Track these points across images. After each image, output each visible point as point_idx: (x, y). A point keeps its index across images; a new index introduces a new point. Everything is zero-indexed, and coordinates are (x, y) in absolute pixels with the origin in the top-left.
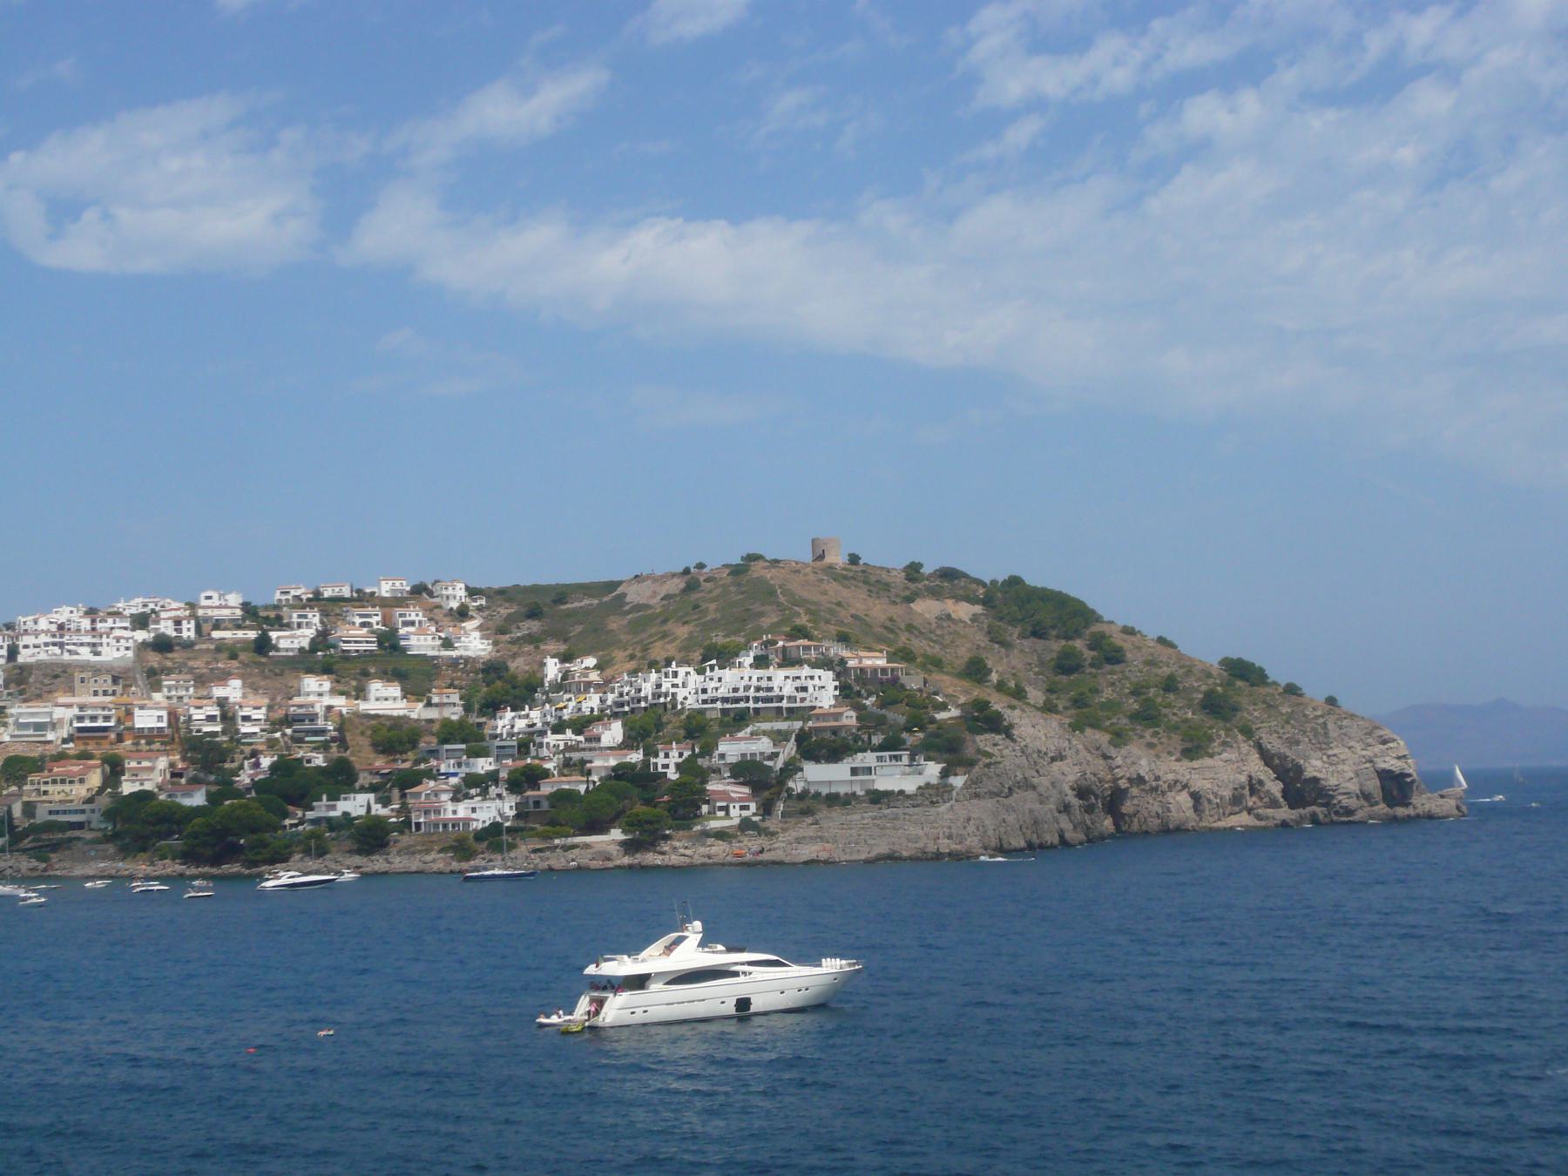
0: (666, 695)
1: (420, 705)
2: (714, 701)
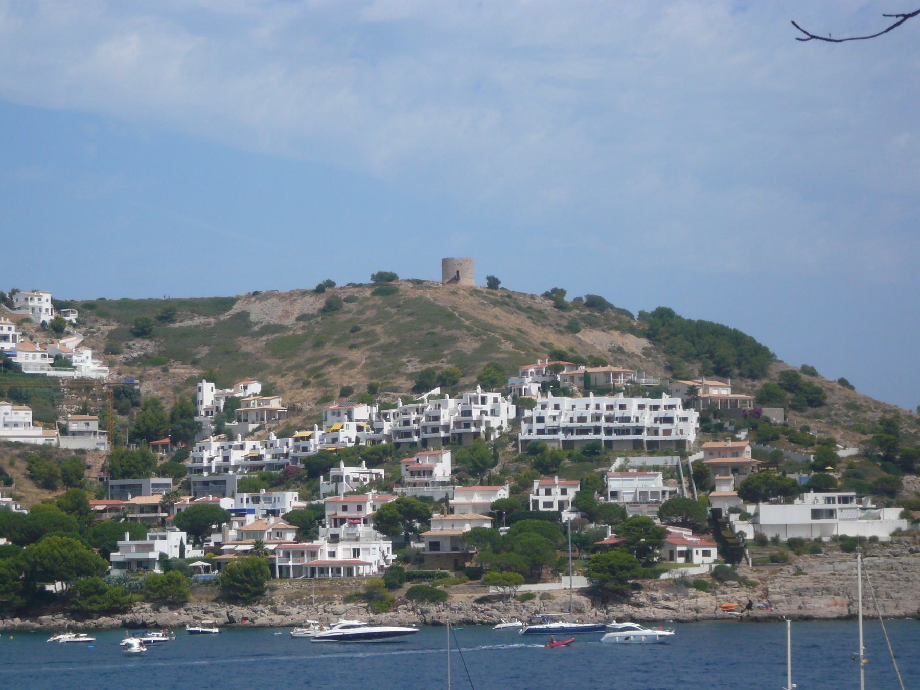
0: (478, 423)
2: (554, 431)
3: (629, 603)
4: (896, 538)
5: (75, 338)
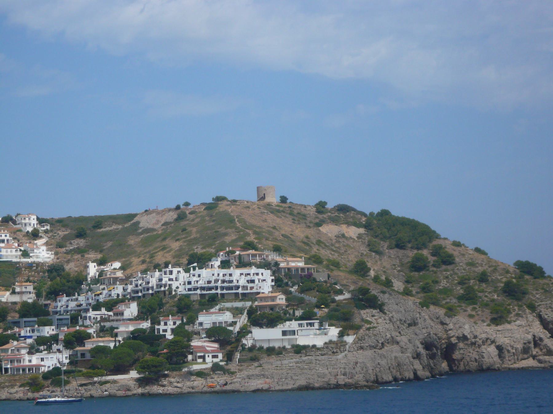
0: (165, 286)
2: (195, 289)
3: (158, 385)
4: (326, 345)
5: (44, 240)
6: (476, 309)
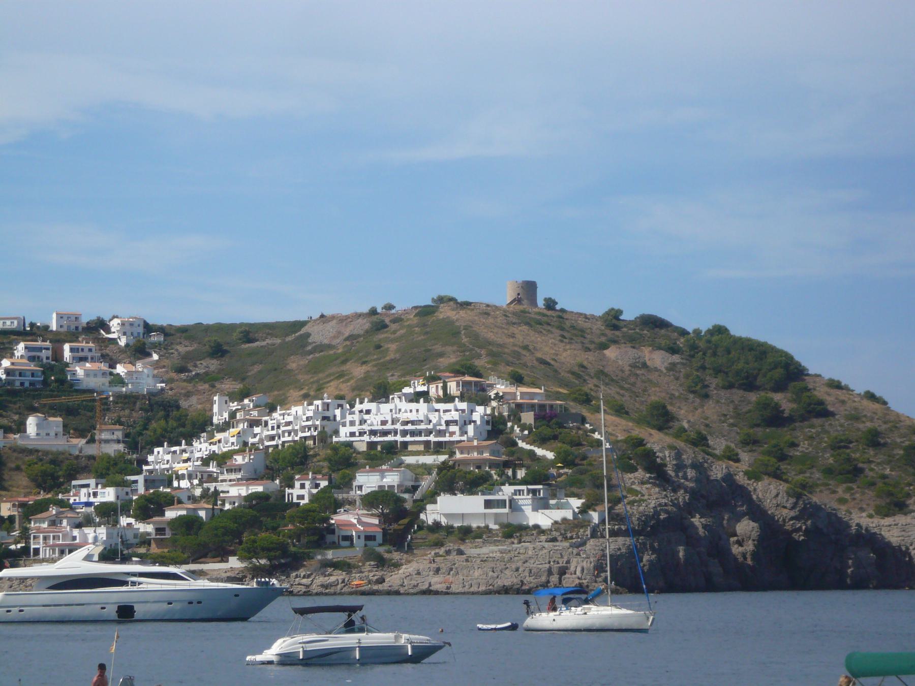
1: (84, 441)
6: (853, 489)
